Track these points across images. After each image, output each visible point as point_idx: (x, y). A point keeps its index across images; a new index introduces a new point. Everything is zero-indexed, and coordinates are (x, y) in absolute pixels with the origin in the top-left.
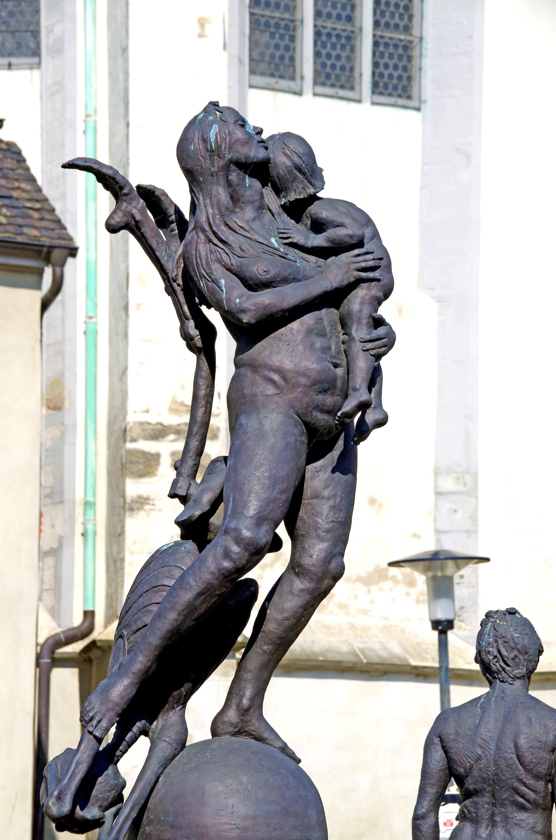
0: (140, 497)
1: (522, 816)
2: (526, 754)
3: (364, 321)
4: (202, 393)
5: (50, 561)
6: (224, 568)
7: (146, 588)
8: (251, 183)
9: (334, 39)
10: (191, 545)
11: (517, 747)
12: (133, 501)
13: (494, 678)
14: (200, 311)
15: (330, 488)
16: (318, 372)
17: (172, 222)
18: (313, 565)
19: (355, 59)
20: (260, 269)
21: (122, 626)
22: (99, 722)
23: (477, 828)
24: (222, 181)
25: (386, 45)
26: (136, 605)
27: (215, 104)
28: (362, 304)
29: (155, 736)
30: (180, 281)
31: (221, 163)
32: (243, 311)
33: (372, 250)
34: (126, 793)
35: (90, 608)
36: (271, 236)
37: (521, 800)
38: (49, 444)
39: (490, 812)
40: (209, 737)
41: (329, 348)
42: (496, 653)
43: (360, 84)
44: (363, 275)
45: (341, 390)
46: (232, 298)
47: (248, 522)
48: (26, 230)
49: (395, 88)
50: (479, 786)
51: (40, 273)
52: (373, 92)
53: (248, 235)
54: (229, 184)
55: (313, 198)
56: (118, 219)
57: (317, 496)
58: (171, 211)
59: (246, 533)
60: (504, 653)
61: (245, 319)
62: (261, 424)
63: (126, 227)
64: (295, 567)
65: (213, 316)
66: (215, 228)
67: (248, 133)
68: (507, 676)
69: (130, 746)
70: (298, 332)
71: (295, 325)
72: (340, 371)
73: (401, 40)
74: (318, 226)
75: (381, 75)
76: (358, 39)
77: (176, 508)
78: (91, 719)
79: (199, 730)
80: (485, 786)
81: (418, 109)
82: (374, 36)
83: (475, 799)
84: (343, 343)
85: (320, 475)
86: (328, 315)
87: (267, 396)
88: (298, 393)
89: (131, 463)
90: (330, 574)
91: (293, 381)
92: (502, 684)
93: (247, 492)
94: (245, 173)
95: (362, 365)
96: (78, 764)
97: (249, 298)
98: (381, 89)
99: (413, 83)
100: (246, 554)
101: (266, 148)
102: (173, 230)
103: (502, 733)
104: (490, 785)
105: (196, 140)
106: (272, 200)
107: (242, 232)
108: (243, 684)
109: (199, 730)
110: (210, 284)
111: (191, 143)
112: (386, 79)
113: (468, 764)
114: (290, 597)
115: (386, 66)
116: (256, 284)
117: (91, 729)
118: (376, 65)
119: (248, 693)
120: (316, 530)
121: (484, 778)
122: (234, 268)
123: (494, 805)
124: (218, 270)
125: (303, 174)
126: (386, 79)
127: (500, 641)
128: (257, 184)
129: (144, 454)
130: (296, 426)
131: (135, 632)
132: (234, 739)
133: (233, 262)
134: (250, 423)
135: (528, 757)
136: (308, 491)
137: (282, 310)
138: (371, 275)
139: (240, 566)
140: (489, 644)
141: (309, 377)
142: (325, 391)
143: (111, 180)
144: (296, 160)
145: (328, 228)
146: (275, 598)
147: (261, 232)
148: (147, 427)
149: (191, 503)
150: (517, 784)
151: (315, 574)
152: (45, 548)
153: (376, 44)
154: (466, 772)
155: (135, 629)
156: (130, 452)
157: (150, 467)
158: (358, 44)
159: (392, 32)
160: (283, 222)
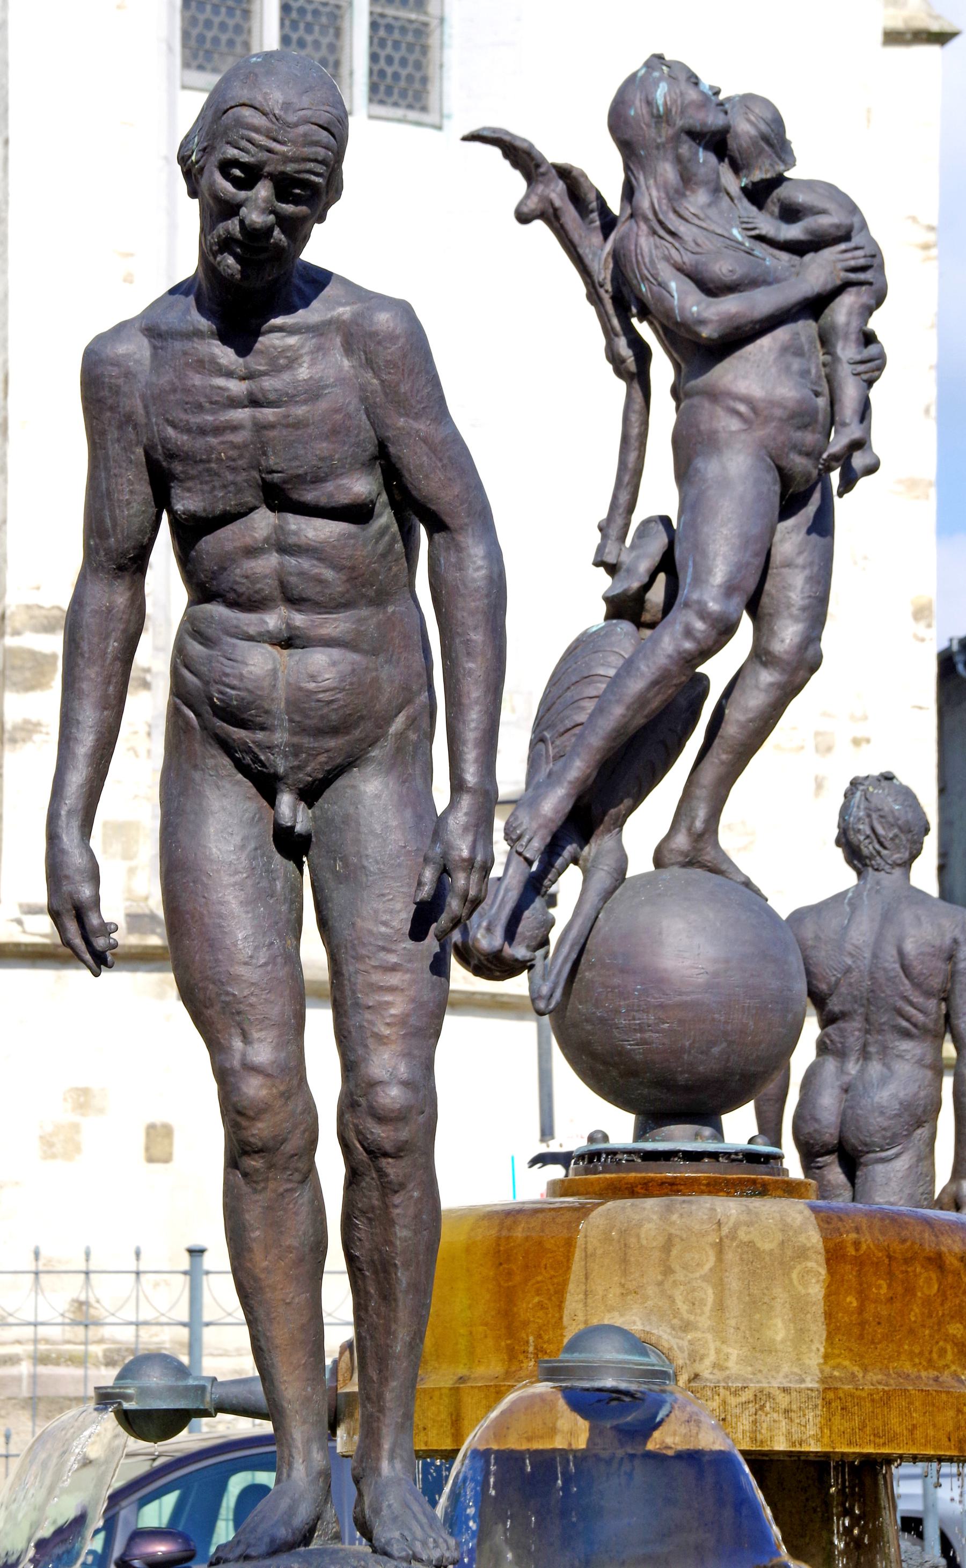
0: (27, 722)
1: (905, 1045)
2: (915, 963)
3: (853, 337)
4: (635, 431)
6: (685, 651)
7: (574, 679)
8: (705, 157)
9: (309, 17)
10: (625, 627)
11: (901, 954)
12: (15, 728)
13: (865, 865)
14: (631, 325)
15: (805, 554)
16: (798, 401)
17: (592, 211)
18: (786, 652)
19: (342, 48)
20: (723, 267)
21: (542, 727)
22: (530, 841)
23: (843, 1063)
24: (670, 156)
25: (389, 28)
26: (561, 700)
27: (660, 57)
28: (850, 314)
29: (589, 865)
30: (609, 287)
31: (671, 132)
32: (702, 322)
33: (861, 245)
34: (554, 936)
36: (732, 227)
37: (905, 1024)
39: (861, 1041)
40: (651, 867)
41: (808, 372)
42: (869, 832)
43: (351, 86)
44: (853, 276)
45: (823, 427)
46: (687, 305)
47: (714, 592)
49: (403, 94)
50: (847, 1007)
52: (371, 100)
53: (704, 225)
54: (679, 160)
55: (779, 180)
56: (533, 204)
57: (788, 565)
58: (592, 196)
59: (713, 606)
60: (880, 831)
61: (706, 332)
62: (724, 468)
63: (542, 216)
64: (760, 654)
65: (644, 330)
66: (661, 217)
67: (703, 93)
68: (883, 863)
69: (560, 874)
70: (770, 350)
71: (765, 342)
72: (822, 402)
73: (411, 21)
74: (790, 213)
75: (382, 74)
76: (347, 16)
77: (603, 582)
78: (520, 837)
79: (640, 863)
80: (856, 1006)
81: (439, 128)
82: (371, 13)
83: (841, 1024)
84: (824, 365)
85: (790, 537)
86: (806, 328)
87: (732, 433)
88: (770, 429)
89: (13, 668)
90: (806, 663)
91: (766, 413)
92: (876, 873)
93: (711, 555)
94: (699, 144)
96: (507, 891)
97: (708, 306)
98: (381, 95)
99: (430, 87)
100: (714, 633)
101: (726, 113)
102: (592, 222)
103: (880, 938)
104: (863, 1005)
105: (637, 103)
106: (731, 182)
108: (695, 803)
109: (640, 863)
110: (656, 288)
111: (630, 107)
112: (389, 80)
113: (833, 979)
114: (755, 693)
115: (389, 60)
116: (717, 288)
117: (520, 850)
118: (374, 58)
119: (701, 813)
120: (788, 608)
121: (854, 997)
122: (687, 267)
123: (867, 1032)
124: (666, 272)
125: (771, 145)
126: (389, 80)
127: (874, 816)
128: (712, 158)
129: (33, 654)
130: (768, 471)
131: (563, 734)
132: (684, 870)
133: (686, 259)
134: (710, 468)
135: (917, 967)
136: (777, 558)
137: (752, 322)
138: (861, 276)
139: (706, 648)
140: (859, 819)
141: (785, 408)
142: (804, 427)
143: (525, 156)
144: (763, 127)
145: (805, 215)
146: (736, 693)
147: (718, 225)
148: (37, 612)
149: (622, 573)
150: (900, 1003)
151: (788, 664)
153: (374, 26)
154: (830, 989)
155: (562, 730)
156: (9, 653)
157: (43, 674)
158: (345, 25)
159: (397, 9)
160: (745, 209)
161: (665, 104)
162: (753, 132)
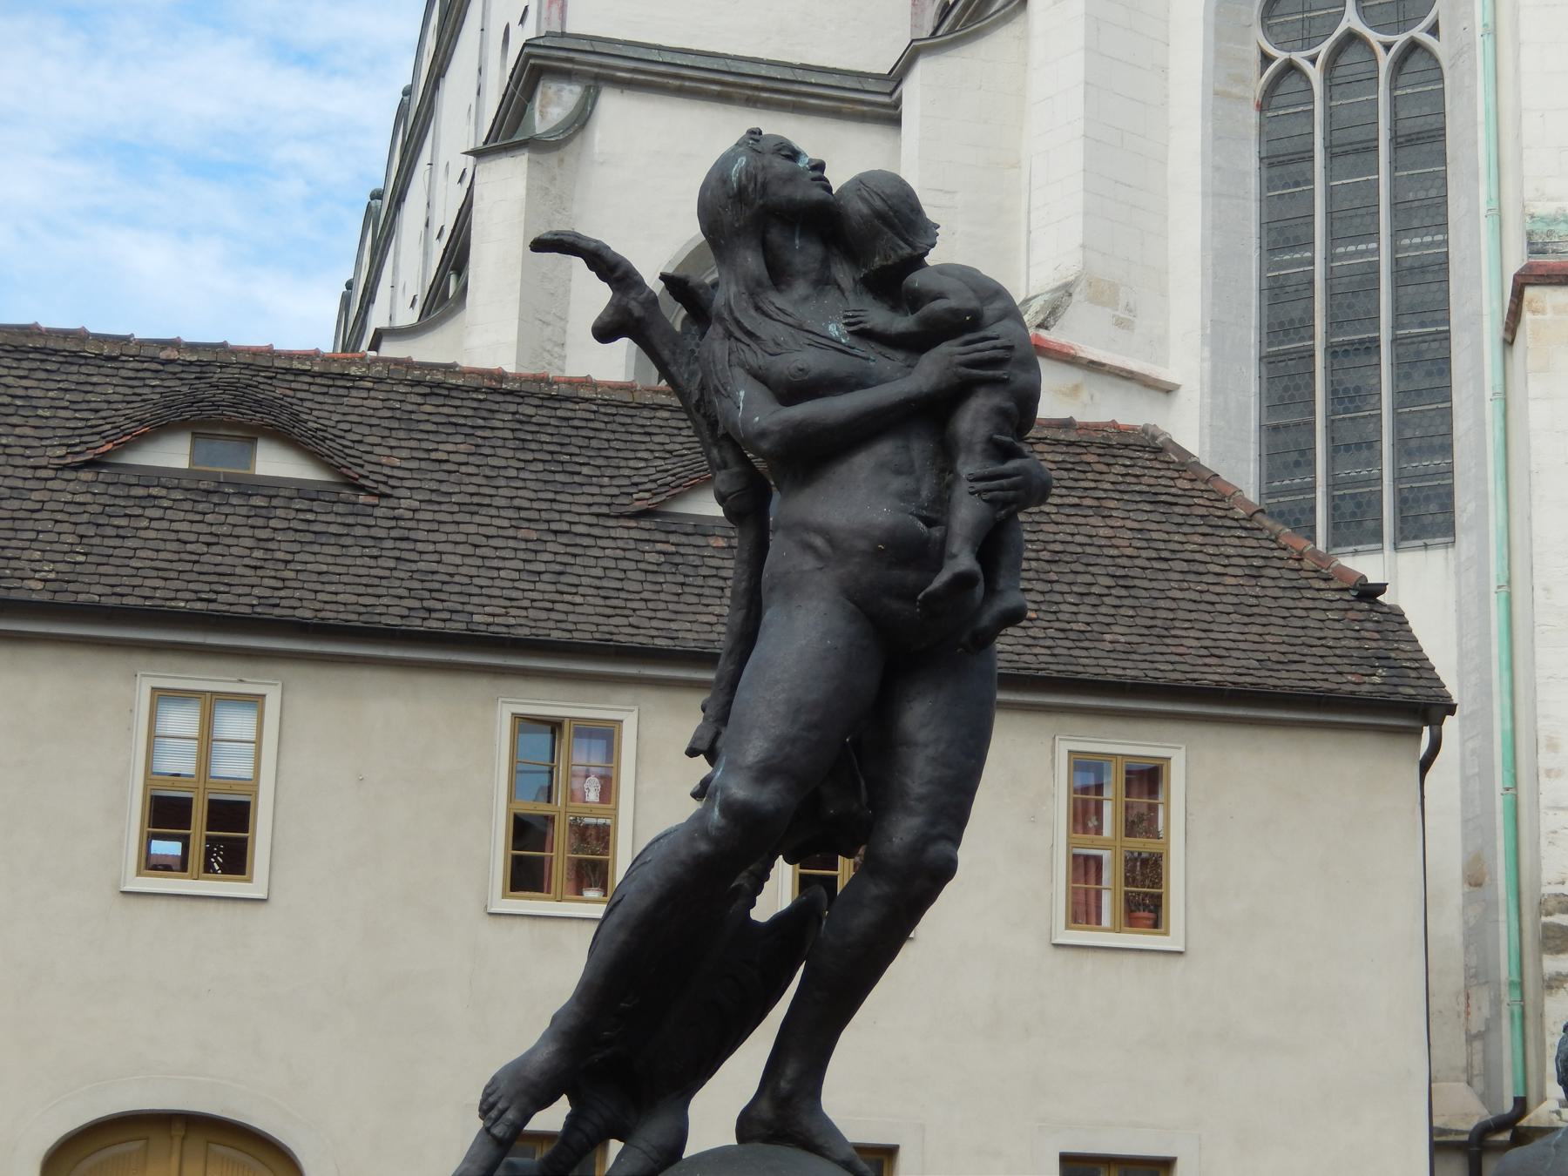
3: (978, 448)
5: (1478, 1045)
8: (803, 253)
35: (1521, 1094)
38: (1472, 922)
41: (917, 493)
48: (1401, 689)
51: (1419, 733)
66: (737, 315)
74: (915, 300)
95: (967, 512)
107: (782, 317)
125: (891, 226)
152: (1474, 1031)
161: (739, 179)
162: (865, 210)
